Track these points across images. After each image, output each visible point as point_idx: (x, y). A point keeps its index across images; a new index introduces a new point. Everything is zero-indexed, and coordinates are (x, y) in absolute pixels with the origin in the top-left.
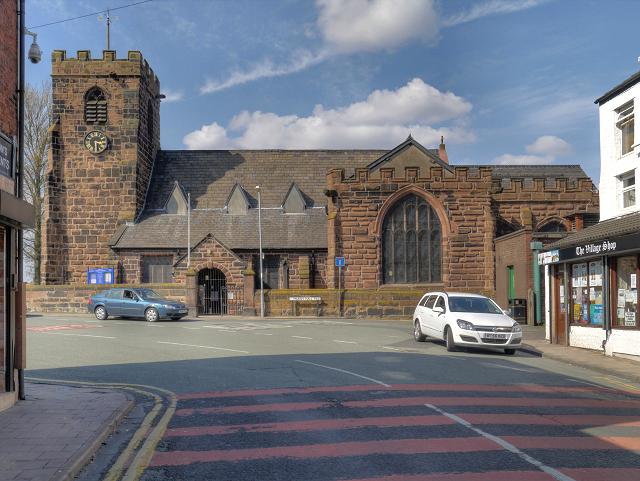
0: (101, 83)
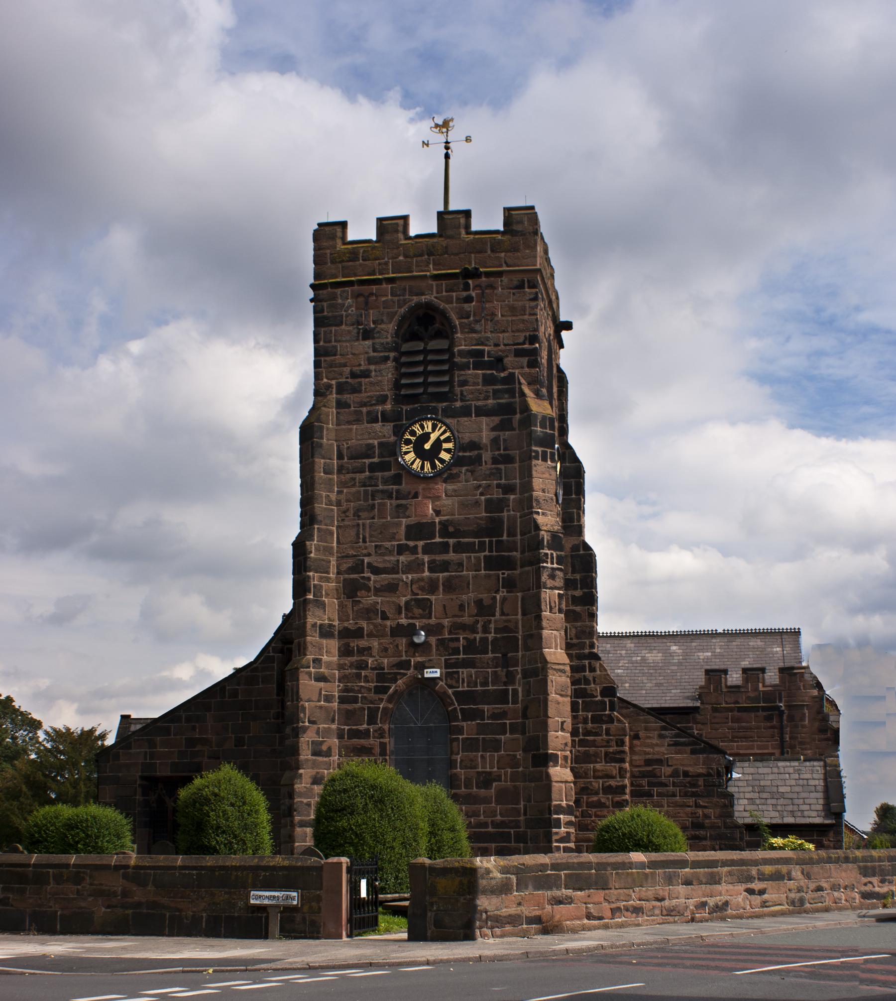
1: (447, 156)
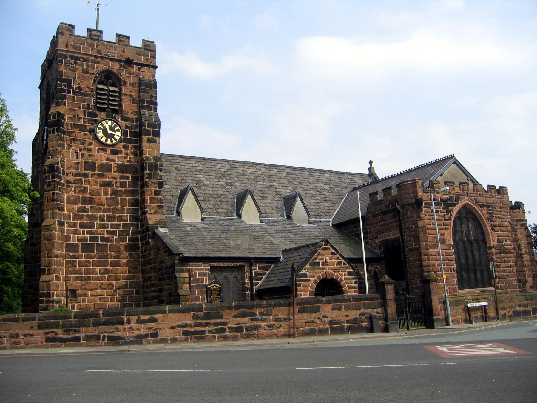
0: (115, 67)
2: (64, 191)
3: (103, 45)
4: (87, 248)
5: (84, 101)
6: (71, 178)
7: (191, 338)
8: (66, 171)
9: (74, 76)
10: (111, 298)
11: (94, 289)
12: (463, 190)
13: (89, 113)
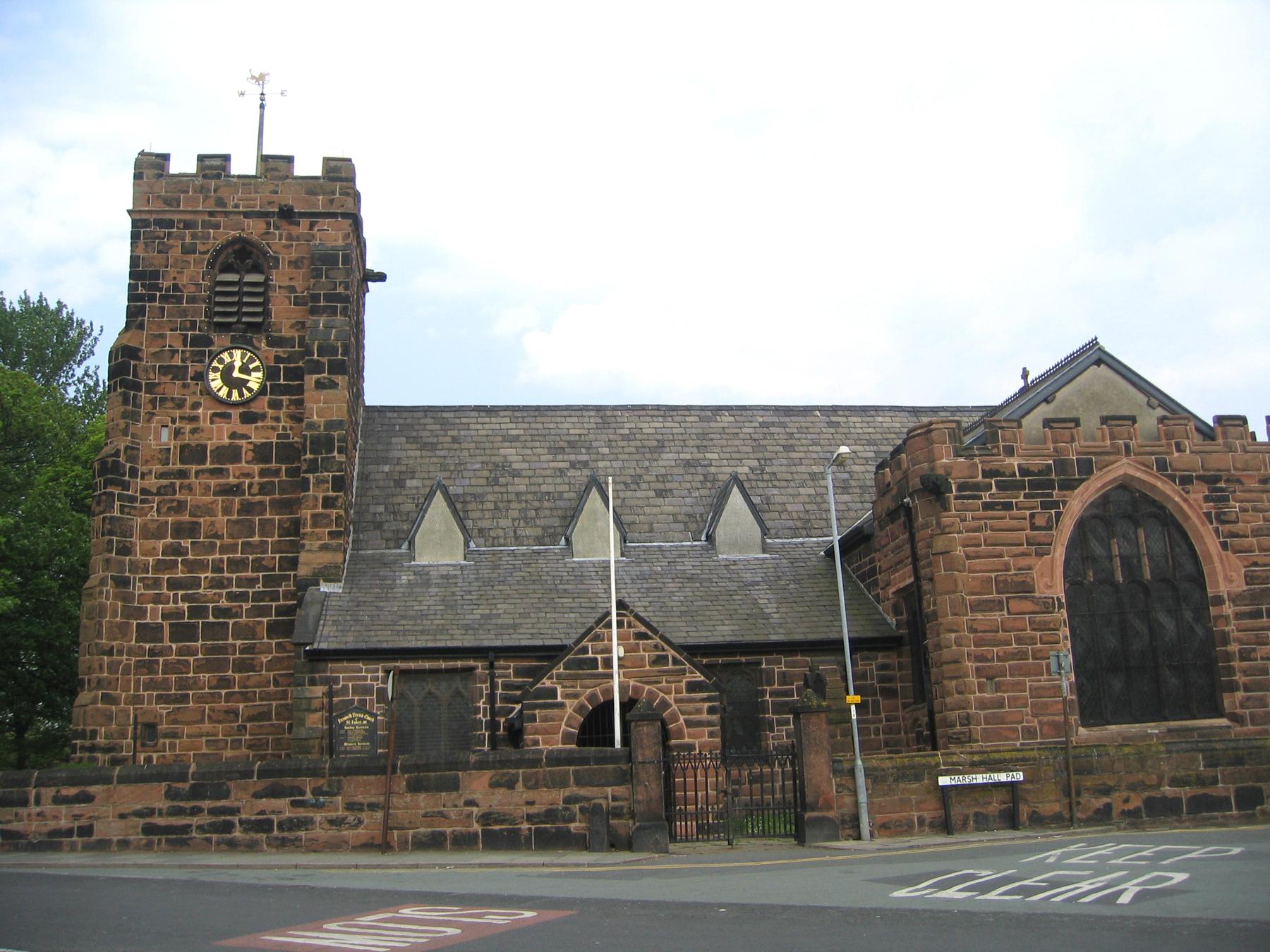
0: (254, 229)
1: (262, 106)
2: (133, 512)
3: (229, 185)
4: (183, 632)
5: (184, 313)
6: (152, 483)
7: (160, 841)
8: (142, 468)
9: (164, 263)
10: (233, 741)
11: (195, 722)
12: (1113, 438)
13: (194, 338)
